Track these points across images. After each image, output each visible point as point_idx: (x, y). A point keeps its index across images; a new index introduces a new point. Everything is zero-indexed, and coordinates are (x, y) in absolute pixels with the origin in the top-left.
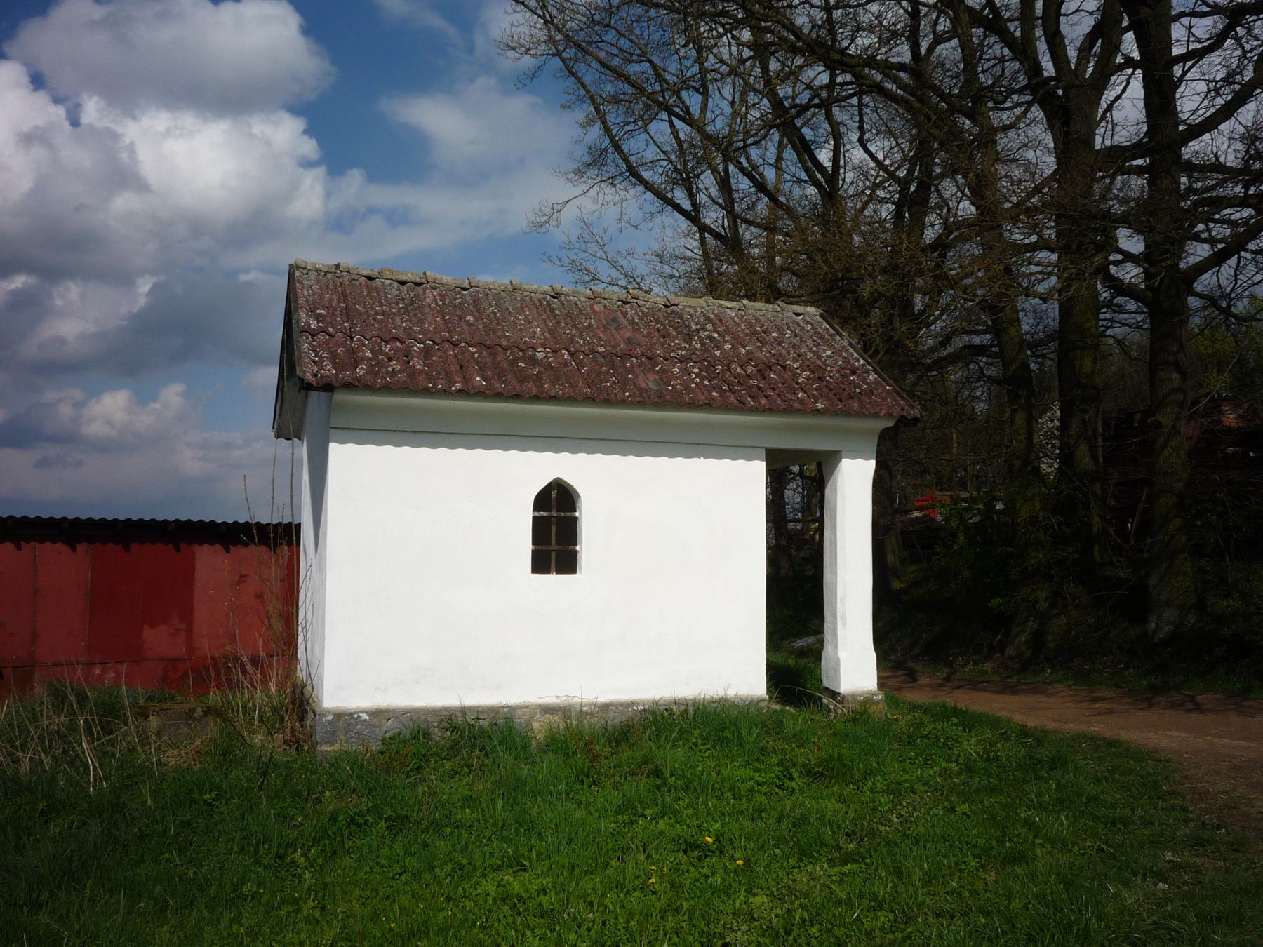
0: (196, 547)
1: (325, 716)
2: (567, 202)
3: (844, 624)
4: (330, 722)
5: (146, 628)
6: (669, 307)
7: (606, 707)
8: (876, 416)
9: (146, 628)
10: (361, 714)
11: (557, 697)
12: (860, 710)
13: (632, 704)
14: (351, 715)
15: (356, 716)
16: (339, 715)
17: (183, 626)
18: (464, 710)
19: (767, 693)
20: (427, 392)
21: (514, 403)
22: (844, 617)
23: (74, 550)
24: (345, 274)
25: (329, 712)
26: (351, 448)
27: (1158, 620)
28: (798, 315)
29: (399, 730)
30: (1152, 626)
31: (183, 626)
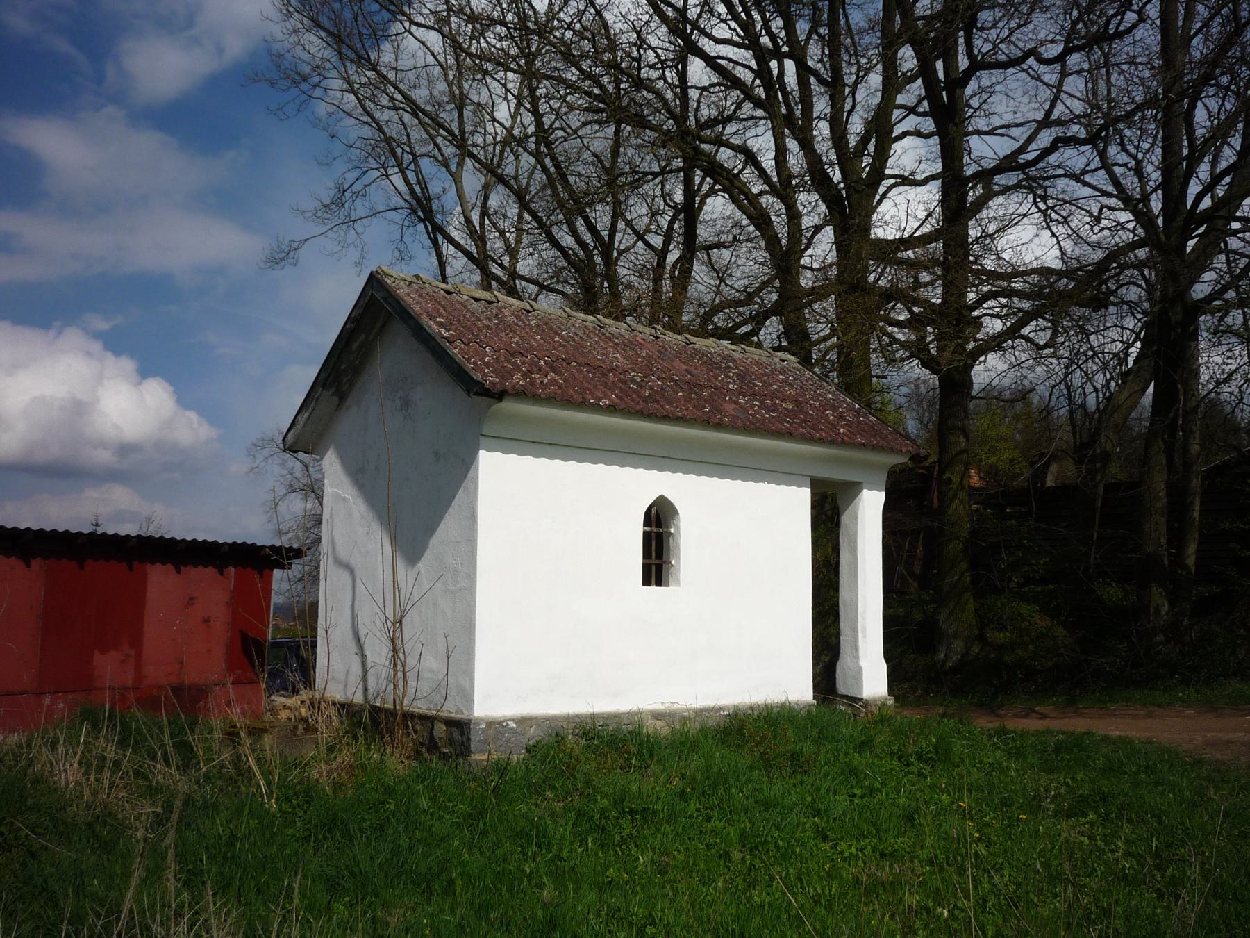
0: (149, 567)
1: (479, 724)
2: (305, 240)
3: (865, 637)
4: (483, 731)
5: (97, 654)
6: (688, 344)
7: (699, 712)
8: (892, 450)
9: (97, 654)
10: (509, 723)
11: (662, 703)
12: (876, 716)
13: (721, 709)
14: (500, 723)
15: (504, 724)
16: (491, 723)
17: (132, 652)
18: (593, 717)
19: (814, 699)
20: (582, 405)
21: (645, 421)
22: (864, 630)
23: (28, 565)
24: (427, 285)
25: (482, 720)
26: (498, 456)
27: (946, 650)
28: (783, 361)
29: (540, 738)
30: (942, 656)
31: (132, 652)
